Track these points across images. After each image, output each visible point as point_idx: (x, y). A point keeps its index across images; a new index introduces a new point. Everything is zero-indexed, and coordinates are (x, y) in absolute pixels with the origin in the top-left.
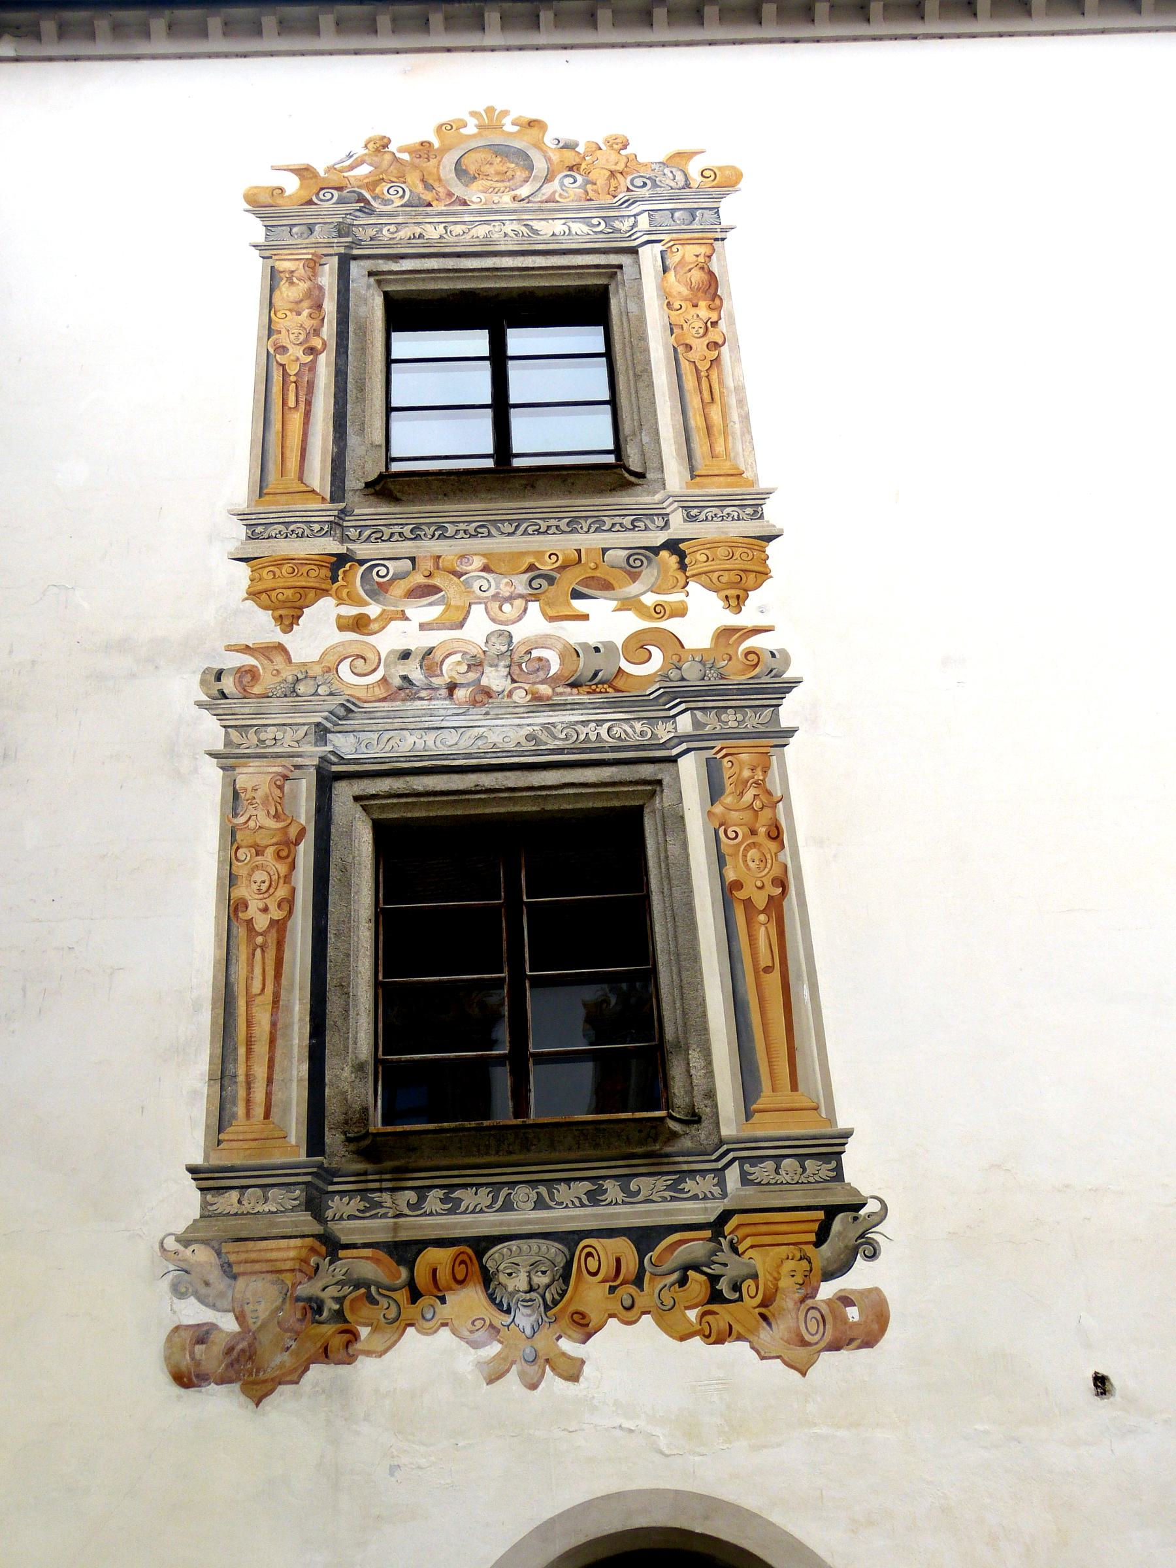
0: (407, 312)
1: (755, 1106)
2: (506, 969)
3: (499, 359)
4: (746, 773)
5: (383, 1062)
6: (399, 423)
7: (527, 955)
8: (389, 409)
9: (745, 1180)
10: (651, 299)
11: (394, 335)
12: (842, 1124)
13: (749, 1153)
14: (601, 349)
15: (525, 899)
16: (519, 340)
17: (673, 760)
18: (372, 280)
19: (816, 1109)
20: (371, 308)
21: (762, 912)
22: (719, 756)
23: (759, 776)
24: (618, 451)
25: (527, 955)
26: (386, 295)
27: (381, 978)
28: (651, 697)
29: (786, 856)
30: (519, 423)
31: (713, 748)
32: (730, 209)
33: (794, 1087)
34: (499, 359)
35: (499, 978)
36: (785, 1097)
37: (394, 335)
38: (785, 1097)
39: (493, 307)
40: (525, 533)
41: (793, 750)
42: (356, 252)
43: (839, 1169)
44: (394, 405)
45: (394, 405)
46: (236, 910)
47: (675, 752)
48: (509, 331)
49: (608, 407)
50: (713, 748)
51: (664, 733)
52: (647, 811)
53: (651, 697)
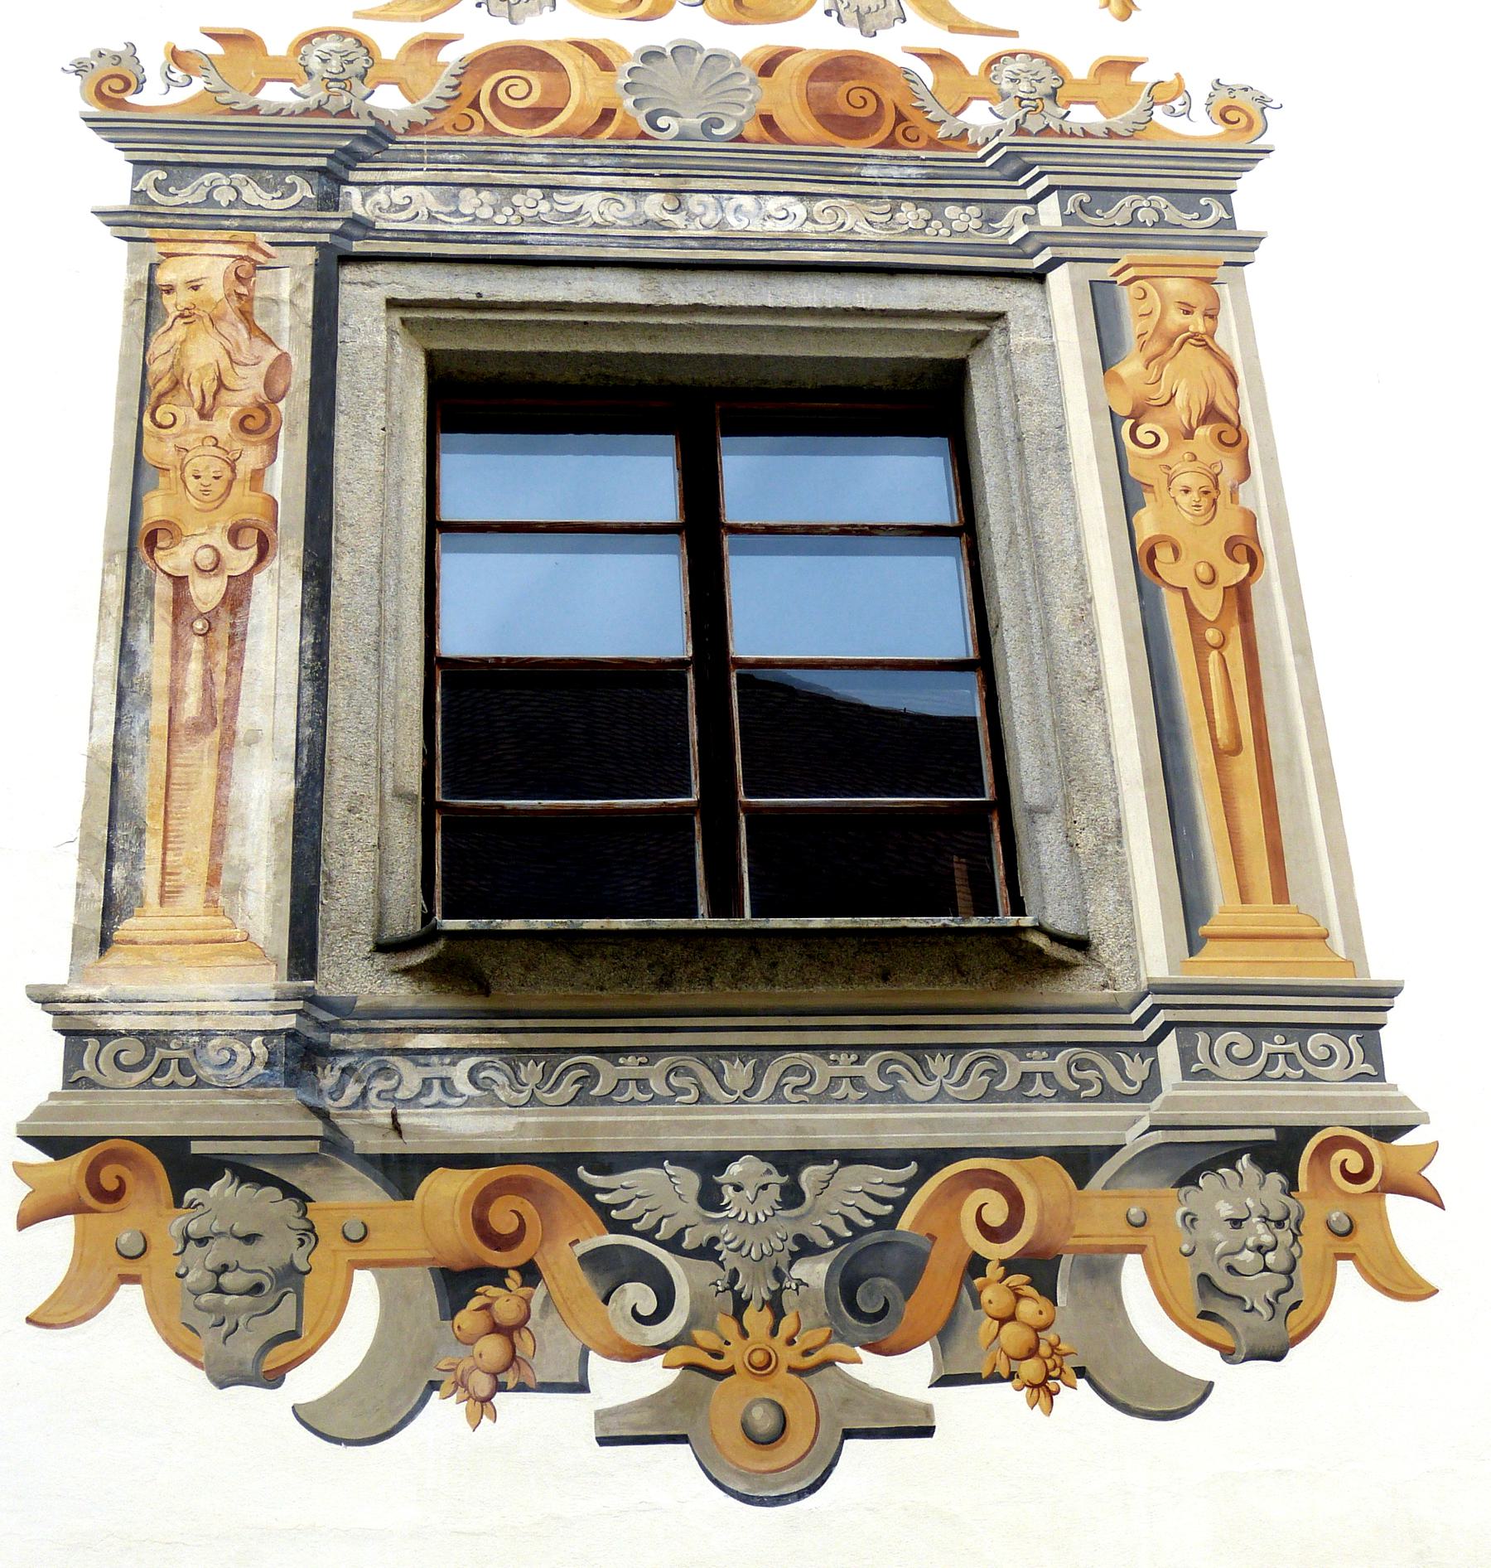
0: (477, 396)
1: (1204, 930)
2: (696, 789)
3: (702, 534)
4: (1176, 318)
6: (459, 566)
7: (735, 693)
8: (435, 526)
9: (1190, 1070)
10: (1049, 368)
11: (444, 439)
12: (1379, 972)
13: (1190, 1014)
14: (944, 513)
15: (742, 797)
16: (758, 478)
17: (1038, 277)
18: (397, 316)
19: (1324, 937)
20: (386, 387)
21: (1213, 624)
22: (1120, 279)
23: (1197, 323)
24: (983, 664)
25: (735, 693)
26: (430, 356)
28: (989, 162)
29: (1256, 495)
30: (747, 578)
31: (1115, 261)
32: (1253, 200)
33: (1281, 893)
34: (702, 534)
35: (682, 808)
36: (1263, 913)
37: (444, 439)
38: (1263, 913)
39: (698, 405)
40: (777, 1096)
41: (1258, 274)
42: (358, 247)
43: (1374, 1054)
44: (446, 514)
45: (446, 514)
47: (1037, 262)
48: (724, 442)
49: (973, 678)
50: (1115, 261)
51: (1013, 226)
52: (978, 376)
53: (989, 162)
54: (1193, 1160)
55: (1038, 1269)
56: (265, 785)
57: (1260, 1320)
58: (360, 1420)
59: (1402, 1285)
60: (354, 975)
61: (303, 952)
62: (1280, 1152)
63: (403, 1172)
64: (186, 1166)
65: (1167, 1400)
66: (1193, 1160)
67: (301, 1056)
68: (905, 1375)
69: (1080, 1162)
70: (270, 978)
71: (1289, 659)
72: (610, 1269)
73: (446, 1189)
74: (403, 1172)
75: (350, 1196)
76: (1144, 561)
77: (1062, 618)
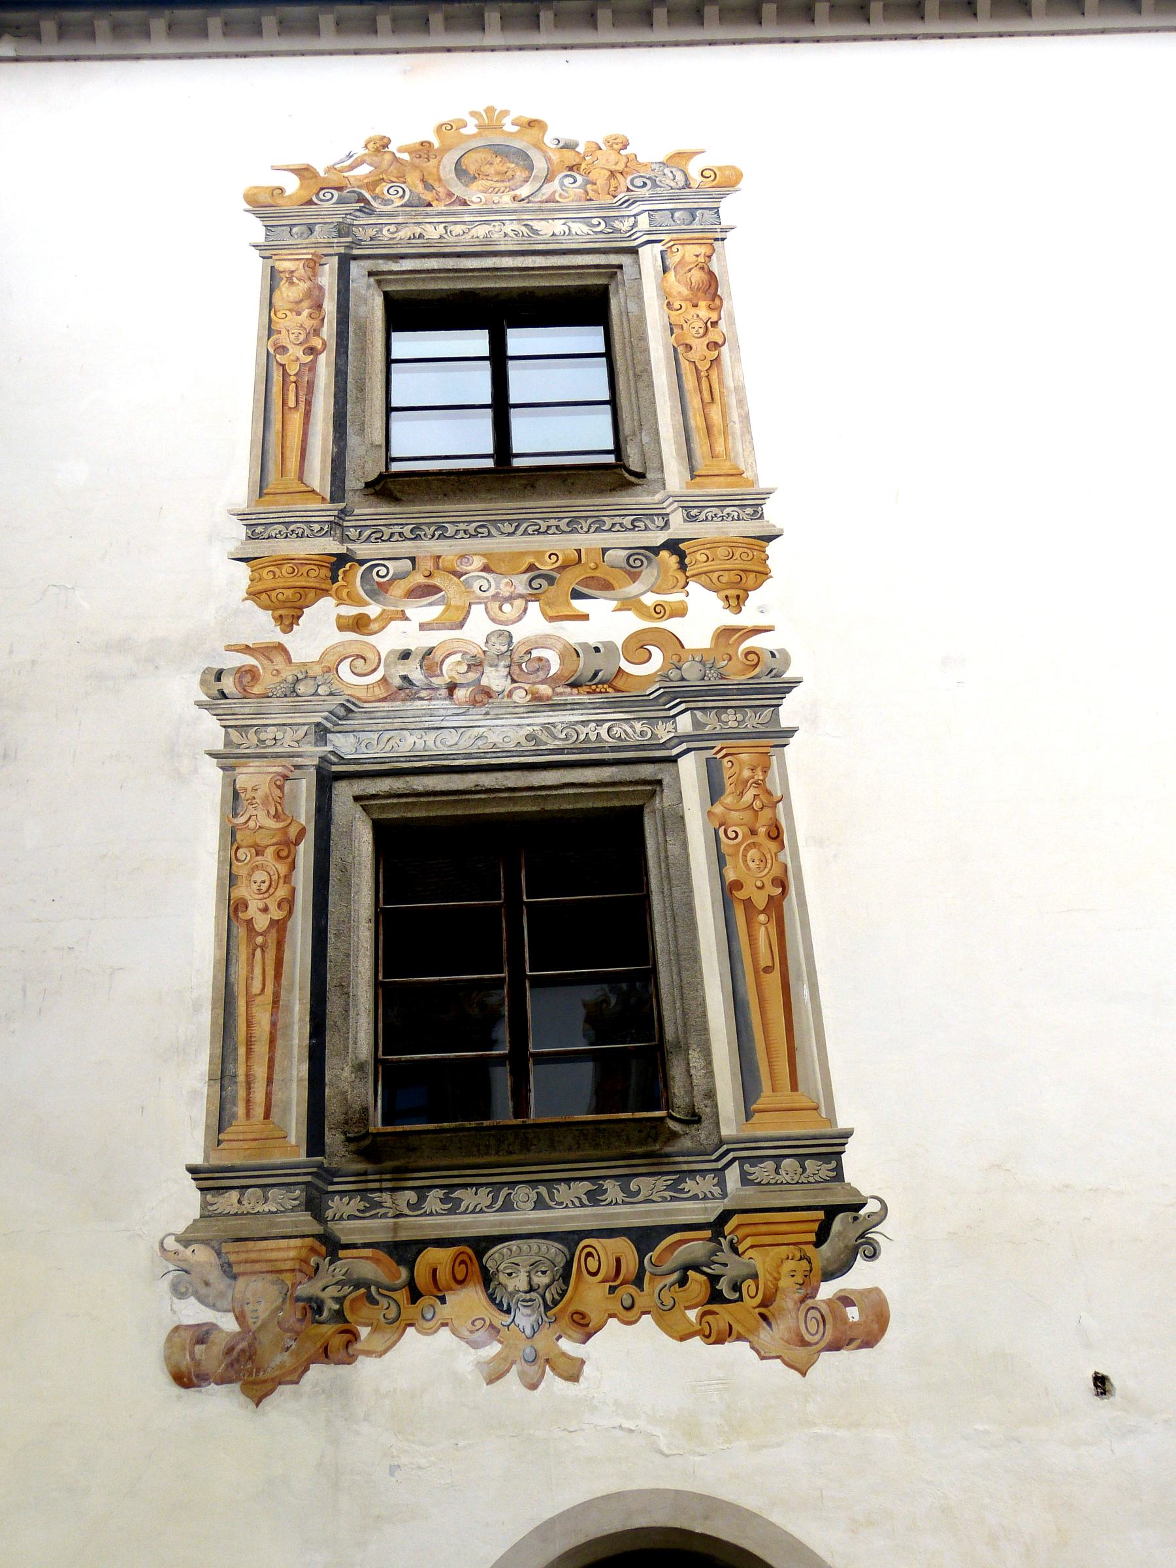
0: (407, 312)
1: (755, 1106)
2: (506, 969)
3: (499, 359)
4: (746, 773)
5: (383, 1062)
6: (399, 423)
7: (527, 955)
8: (389, 409)
9: (745, 1180)
10: (651, 299)
11: (394, 335)
12: (842, 1124)
13: (749, 1153)
14: (601, 349)
15: (525, 899)
16: (519, 340)
17: (673, 760)
18: (372, 280)
19: (816, 1109)
20: (371, 308)
21: (762, 912)
22: (719, 756)
23: (759, 776)
24: (618, 451)
25: (527, 955)
26: (386, 295)
27: (381, 978)
28: (651, 697)
29: (786, 856)
30: (519, 423)
31: (713, 748)
32: (730, 209)
33: (794, 1087)
34: (499, 359)
35: (499, 978)
36: (785, 1097)
37: (394, 335)
38: (785, 1097)
39: (493, 307)
40: (525, 533)
41: (793, 750)
42: (356, 252)
43: (839, 1169)
44: (394, 405)
45: (394, 405)
47: (675, 752)
48: (509, 331)
49: (608, 407)
50: (713, 748)
51: (664, 733)
52: (647, 811)
53: (651, 697)
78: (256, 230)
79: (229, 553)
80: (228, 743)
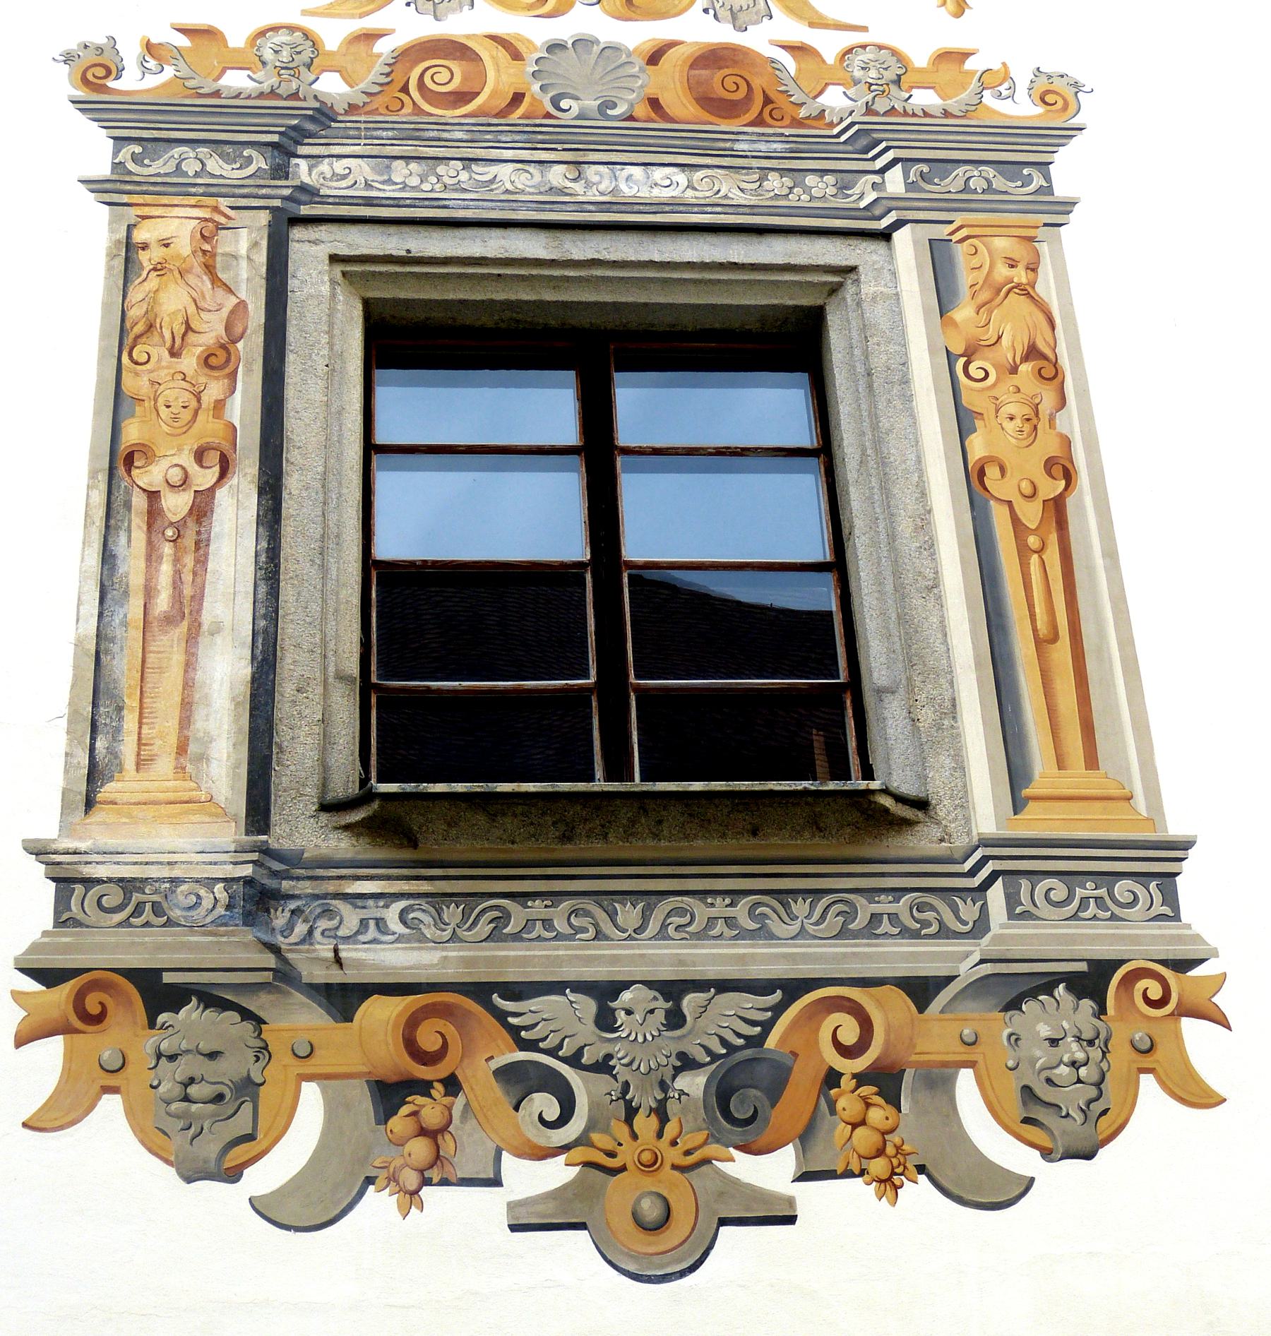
0: (407, 338)
1: (1026, 792)
2: (593, 672)
3: (599, 455)
4: (1002, 271)
5: (377, 688)
6: (391, 482)
7: (626, 590)
8: (371, 448)
9: (1015, 912)
11: (378, 374)
12: (1175, 828)
13: (1014, 864)
14: (805, 437)
15: (632, 679)
16: (646, 407)
17: (885, 236)
18: (338, 269)
19: (1129, 798)
20: (329, 329)
21: (1034, 532)
22: (955, 238)
23: (1020, 275)
24: (838, 565)
25: (626, 590)
26: (367, 303)
27: (374, 679)
28: (843, 138)
29: (1070, 421)
30: (637, 492)
31: (951, 222)
32: (1068, 171)
33: (1092, 761)
34: (599, 455)
35: (581, 689)
36: (1077, 778)
37: (378, 374)
38: (1077, 778)
40: (662, 934)
42: (305, 210)
43: (1171, 898)
44: (381, 438)
45: (381, 438)
46: (129, 460)
47: (884, 223)
48: (618, 377)
49: (830, 578)
50: (951, 222)
51: (864, 193)
52: (834, 320)
53: (843, 138)
54: (1017, 988)
55: (885, 1081)
56: (226, 669)
57: (1074, 1124)
58: (307, 1210)
59: (1195, 1095)
60: (302, 830)
61: (259, 811)
62: (1092, 981)
63: (343, 999)
64: (158, 993)
65: (995, 1193)
66: (1017, 988)
67: (257, 900)
68: (771, 1172)
69: (921, 990)
70: (230, 834)
71: (1099, 562)
72: (520, 1081)
73: (381, 1013)
74: (343, 999)
75: (298, 1019)
76: (975, 478)
77: (905, 527)
78: (95, 150)
79: (17, 960)
80: (117, 166)
